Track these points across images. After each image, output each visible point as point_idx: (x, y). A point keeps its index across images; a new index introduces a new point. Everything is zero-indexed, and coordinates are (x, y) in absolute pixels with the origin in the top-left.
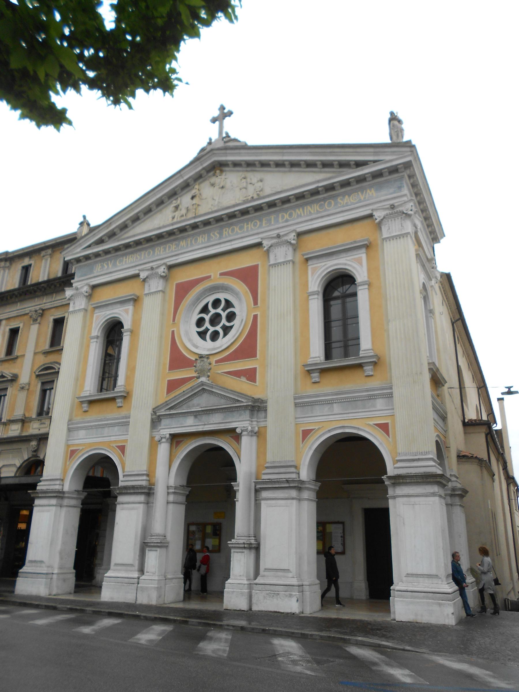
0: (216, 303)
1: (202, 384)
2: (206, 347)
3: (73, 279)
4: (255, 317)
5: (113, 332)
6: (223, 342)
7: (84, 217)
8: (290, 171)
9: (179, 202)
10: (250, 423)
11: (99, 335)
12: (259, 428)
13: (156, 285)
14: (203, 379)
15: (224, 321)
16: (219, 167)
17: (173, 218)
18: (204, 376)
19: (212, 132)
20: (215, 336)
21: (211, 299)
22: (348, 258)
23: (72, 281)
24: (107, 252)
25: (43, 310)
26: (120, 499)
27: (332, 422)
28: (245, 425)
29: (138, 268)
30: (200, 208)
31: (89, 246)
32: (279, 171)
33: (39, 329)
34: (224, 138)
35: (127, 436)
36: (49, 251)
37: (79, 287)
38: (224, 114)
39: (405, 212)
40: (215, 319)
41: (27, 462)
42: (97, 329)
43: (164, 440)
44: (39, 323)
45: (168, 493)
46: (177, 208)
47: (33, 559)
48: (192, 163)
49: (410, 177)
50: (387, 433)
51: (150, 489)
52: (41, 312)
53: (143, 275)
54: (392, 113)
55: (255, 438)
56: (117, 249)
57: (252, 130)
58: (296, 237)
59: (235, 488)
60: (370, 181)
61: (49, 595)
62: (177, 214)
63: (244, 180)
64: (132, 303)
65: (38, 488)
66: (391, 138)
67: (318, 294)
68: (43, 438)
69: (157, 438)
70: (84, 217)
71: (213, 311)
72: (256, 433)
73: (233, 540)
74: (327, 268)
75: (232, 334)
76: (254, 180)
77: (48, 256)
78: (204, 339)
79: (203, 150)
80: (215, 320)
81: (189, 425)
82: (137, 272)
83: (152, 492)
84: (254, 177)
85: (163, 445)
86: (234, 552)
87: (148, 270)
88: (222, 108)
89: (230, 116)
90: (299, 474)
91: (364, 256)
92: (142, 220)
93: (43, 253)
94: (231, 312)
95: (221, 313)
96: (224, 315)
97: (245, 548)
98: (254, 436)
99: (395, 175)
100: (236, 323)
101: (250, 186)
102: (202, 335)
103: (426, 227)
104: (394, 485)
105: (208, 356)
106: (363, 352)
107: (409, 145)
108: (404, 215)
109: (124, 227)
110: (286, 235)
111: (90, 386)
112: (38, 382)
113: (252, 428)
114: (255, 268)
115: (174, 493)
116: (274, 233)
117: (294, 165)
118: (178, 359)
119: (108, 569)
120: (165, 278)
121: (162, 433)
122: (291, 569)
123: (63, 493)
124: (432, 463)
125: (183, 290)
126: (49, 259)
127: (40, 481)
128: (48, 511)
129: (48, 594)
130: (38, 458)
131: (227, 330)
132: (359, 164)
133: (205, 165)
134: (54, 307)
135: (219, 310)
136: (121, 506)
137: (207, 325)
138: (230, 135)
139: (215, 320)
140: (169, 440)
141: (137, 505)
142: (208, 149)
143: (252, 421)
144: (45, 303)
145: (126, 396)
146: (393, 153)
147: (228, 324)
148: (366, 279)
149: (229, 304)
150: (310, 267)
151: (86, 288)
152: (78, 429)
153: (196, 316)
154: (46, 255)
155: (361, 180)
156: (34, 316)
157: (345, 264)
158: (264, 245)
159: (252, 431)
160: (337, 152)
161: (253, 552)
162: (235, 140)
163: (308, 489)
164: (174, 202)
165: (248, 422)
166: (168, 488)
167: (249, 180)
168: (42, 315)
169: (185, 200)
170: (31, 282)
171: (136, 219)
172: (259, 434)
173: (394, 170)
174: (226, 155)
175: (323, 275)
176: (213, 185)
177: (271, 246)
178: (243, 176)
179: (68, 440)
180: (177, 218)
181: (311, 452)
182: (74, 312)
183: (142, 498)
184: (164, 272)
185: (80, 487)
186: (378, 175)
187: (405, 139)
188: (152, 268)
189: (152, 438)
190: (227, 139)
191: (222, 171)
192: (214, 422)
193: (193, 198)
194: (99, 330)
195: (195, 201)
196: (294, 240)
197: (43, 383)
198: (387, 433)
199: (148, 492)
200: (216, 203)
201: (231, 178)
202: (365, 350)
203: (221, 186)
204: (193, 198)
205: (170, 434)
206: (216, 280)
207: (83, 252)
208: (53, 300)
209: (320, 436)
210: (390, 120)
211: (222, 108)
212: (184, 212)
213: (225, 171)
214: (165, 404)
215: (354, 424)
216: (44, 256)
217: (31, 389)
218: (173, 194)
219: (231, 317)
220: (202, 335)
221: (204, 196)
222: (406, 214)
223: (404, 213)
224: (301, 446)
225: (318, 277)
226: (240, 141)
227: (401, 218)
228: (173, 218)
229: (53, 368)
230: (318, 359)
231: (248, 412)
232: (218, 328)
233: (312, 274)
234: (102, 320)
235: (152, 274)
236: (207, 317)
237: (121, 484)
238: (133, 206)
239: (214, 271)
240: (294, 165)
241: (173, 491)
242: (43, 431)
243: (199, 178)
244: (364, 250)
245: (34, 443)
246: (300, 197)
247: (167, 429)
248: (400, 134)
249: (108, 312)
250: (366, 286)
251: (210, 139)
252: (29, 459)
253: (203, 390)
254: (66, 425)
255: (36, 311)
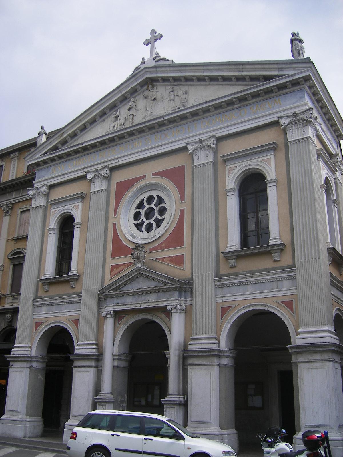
0: (150, 199)
1: (139, 269)
2: (142, 237)
3: (34, 180)
4: (182, 211)
5: (67, 224)
6: (156, 233)
7: (42, 128)
8: (209, 84)
9: (118, 113)
10: (179, 302)
11: (55, 227)
12: (185, 306)
13: (100, 185)
14: (139, 265)
15: (157, 215)
16: (150, 82)
17: (114, 127)
18: (140, 262)
19: (146, 53)
20: (149, 228)
21: (146, 196)
22: (259, 159)
23: (33, 182)
24: (60, 157)
25: (13, 204)
26: (76, 364)
27: (247, 297)
28: (174, 304)
29: (86, 170)
30: (135, 118)
31: (46, 152)
32: (201, 85)
33: (10, 220)
34: (155, 57)
35: (79, 312)
36: (17, 154)
37: (39, 187)
38: (155, 37)
39: (306, 119)
40: (149, 214)
41: (4, 331)
42: (53, 223)
43: (109, 316)
44: (10, 215)
45: (114, 360)
46: (117, 117)
47: (10, 409)
48: (128, 80)
49: (310, 87)
50: (292, 310)
51: (99, 356)
52: (11, 205)
53: (90, 176)
54: (293, 34)
55: (183, 315)
56: (68, 154)
57: (177, 51)
58: (215, 142)
59: (167, 356)
60: (276, 92)
61: (24, 437)
62: (117, 123)
63: (172, 93)
64: (80, 200)
65: (12, 353)
66: (293, 56)
67: (234, 191)
68: (15, 311)
69: (104, 314)
70: (42, 128)
71: (147, 206)
72: (183, 310)
73: (165, 398)
74: (241, 169)
75: (164, 225)
76: (181, 93)
77: (16, 158)
78: (141, 231)
79: (137, 68)
80: (149, 214)
81: (129, 303)
82: (85, 173)
83: (100, 358)
84: (180, 90)
85: (108, 319)
86: (167, 407)
87: (93, 172)
88: (154, 32)
89: (160, 39)
90: (219, 344)
91: (272, 157)
92: (88, 129)
93: (12, 156)
94: (162, 206)
95: (155, 207)
96: (156, 209)
97: (175, 404)
98: (182, 313)
99: (297, 88)
100: (167, 216)
101: (176, 97)
102: (139, 227)
103: (330, 127)
104: (297, 353)
105: (143, 246)
106: (271, 241)
107: (308, 61)
108: (305, 122)
109: (74, 135)
110: (207, 140)
111: (49, 269)
112: (10, 265)
113: (180, 306)
114: (182, 168)
115: (118, 359)
116: (197, 138)
117: (213, 79)
118: (119, 248)
119: (68, 418)
120: (108, 179)
121: (107, 310)
122: (212, 421)
123: (32, 357)
124: (328, 334)
125: (123, 188)
126: (17, 160)
127: (14, 348)
128: (20, 372)
129: (23, 437)
130: (13, 328)
131: (159, 222)
132: (267, 78)
133: (139, 81)
134: (21, 201)
135: (153, 206)
136: (76, 369)
137: (143, 218)
138: (160, 55)
139: (149, 214)
140: (113, 316)
141: (89, 369)
142: (142, 67)
143: (180, 300)
144: (14, 198)
145: (77, 279)
146: (295, 69)
147: (160, 217)
148: (274, 177)
149: (160, 200)
150: (227, 167)
151: (45, 188)
152: (40, 306)
153: (133, 211)
154: (14, 157)
155: (268, 91)
156: (6, 209)
157: (257, 165)
158: (189, 149)
159: (180, 309)
160: (248, 68)
161: (182, 407)
162: (165, 59)
163: (227, 357)
164: (115, 113)
165: (177, 301)
166: (113, 355)
167: (176, 93)
168: (12, 208)
169: (123, 112)
170: (3, 181)
171: (84, 128)
172: (187, 311)
173: (295, 83)
174: (157, 72)
175: (238, 173)
176: (146, 97)
177: (195, 149)
178: (171, 89)
179: (33, 315)
180: (117, 127)
181: (229, 326)
182: (37, 208)
183: (93, 363)
184: (106, 174)
185: (45, 354)
186: (281, 87)
187: (305, 57)
188: (97, 171)
189: (99, 313)
190: (157, 59)
191: (153, 86)
192: (150, 301)
193: (129, 109)
194: (55, 223)
195: (131, 112)
196: (213, 144)
197: (14, 266)
198: (292, 310)
199: (98, 358)
200: (149, 113)
201: (161, 91)
202: (273, 239)
203: (153, 98)
204: (129, 109)
205: (114, 311)
206: (150, 180)
207: (41, 157)
208: (21, 195)
209: (236, 313)
210: (292, 41)
211: (154, 32)
212: (122, 121)
213: (157, 85)
214: (108, 286)
215: (264, 302)
216: (13, 158)
217: (5, 270)
218: (113, 107)
219: (163, 211)
220: (139, 227)
221: (139, 108)
222: (306, 120)
223: (305, 120)
224: (221, 321)
225: (234, 176)
226: (168, 60)
227: (303, 124)
228: (114, 127)
229: (21, 253)
230: (235, 247)
231: (176, 293)
232: (152, 221)
233: (229, 172)
234: (57, 215)
235: (97, 175)
236: (143, 212)
237: (76, 352)
238: (81, 118)
239: (147, 170)
240: (213, 79)
241: (117, 357)
242: (15, 306)
243: (134, 91)
244: (272, 152)
245: (9, 315)
246: (218, 107)
247: (109, 308)
248: (301, 52)
249: (62, 208)
250: (275, 184)
251: (144, 59)
252: (5, 328)
253: (140, 275)
254: (32, 303)
255: (7, 205)
